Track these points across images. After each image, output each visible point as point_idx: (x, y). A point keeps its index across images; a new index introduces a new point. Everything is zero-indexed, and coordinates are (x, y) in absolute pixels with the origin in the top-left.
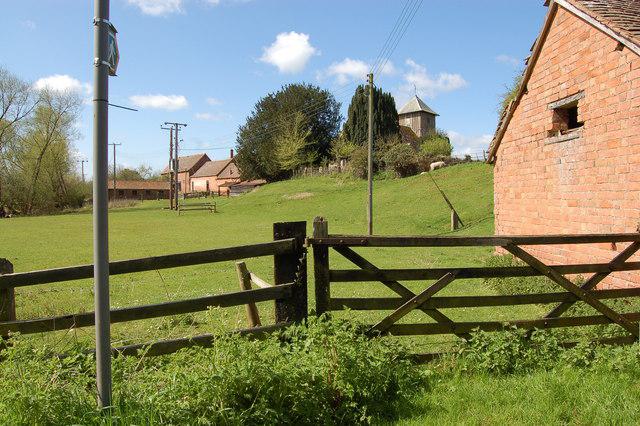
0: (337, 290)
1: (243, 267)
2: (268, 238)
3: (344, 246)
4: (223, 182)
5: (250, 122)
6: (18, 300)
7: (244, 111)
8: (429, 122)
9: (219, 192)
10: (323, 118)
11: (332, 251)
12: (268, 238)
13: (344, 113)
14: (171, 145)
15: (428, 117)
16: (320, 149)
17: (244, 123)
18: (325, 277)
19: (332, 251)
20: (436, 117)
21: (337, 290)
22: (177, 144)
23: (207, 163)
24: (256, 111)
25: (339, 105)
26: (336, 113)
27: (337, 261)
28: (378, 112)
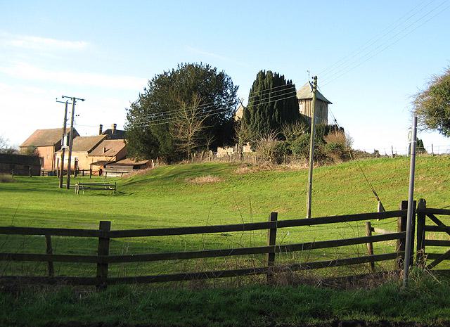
0: (429, 236)
1: (369, 224)
2: (97, 228)
3: (432, 213)
4: (96, 159)
5: (142, 98)
6: (111, 245)
7: (137, 86)
8: (321, 110)
9: (91, 170)
10: (219, 100)
11: (427, 218)
12: (97, 228)
13: (244, 96)
14: (66, 119)
15: (322, 103)
16: (220, 132)
17: (135, 99)
18: (423, 228)
19: (427, 218)
20: (329, 105)
21: (429, 236)
22: (73, 118)
23: (77, 137)
24: (148, 88)
25: (237, 88)
26: (234, 95)
27: (429, 222)
28: (276, 99)
